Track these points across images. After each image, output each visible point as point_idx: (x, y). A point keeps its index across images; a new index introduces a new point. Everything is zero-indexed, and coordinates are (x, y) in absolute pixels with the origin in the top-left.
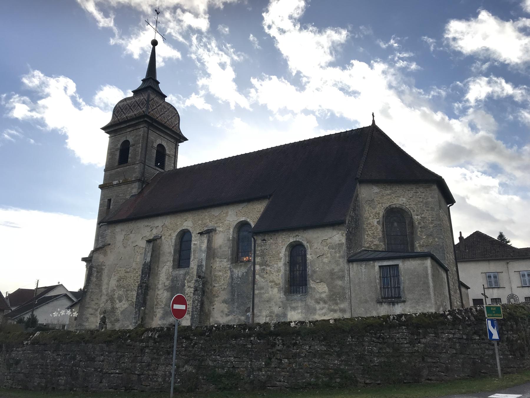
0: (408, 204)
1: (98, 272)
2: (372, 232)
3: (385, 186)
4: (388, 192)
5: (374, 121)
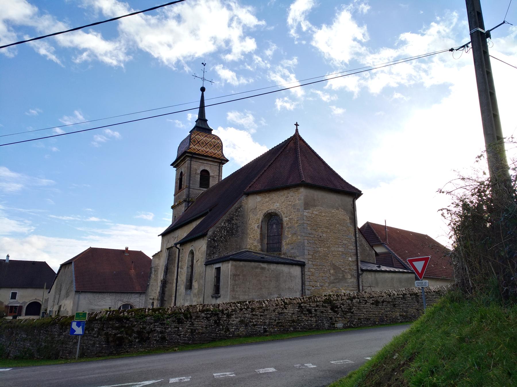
0: (280, 207)
1: (155, 271)
2: (253, 236)
3: (265, 195)
4: (267, 199)
5: (297, 130)
